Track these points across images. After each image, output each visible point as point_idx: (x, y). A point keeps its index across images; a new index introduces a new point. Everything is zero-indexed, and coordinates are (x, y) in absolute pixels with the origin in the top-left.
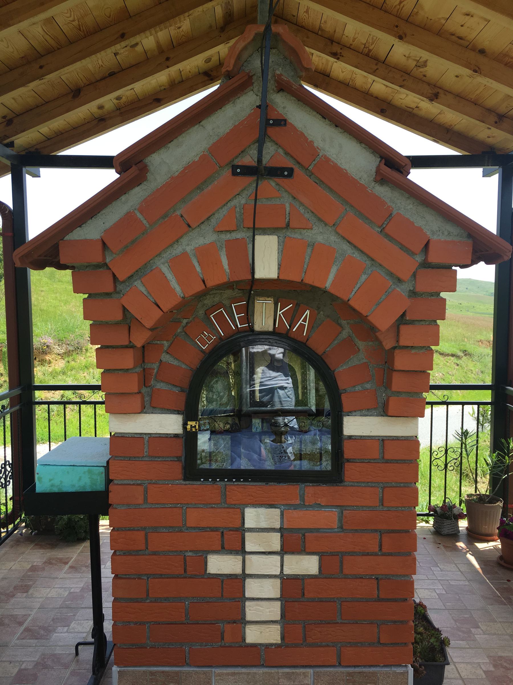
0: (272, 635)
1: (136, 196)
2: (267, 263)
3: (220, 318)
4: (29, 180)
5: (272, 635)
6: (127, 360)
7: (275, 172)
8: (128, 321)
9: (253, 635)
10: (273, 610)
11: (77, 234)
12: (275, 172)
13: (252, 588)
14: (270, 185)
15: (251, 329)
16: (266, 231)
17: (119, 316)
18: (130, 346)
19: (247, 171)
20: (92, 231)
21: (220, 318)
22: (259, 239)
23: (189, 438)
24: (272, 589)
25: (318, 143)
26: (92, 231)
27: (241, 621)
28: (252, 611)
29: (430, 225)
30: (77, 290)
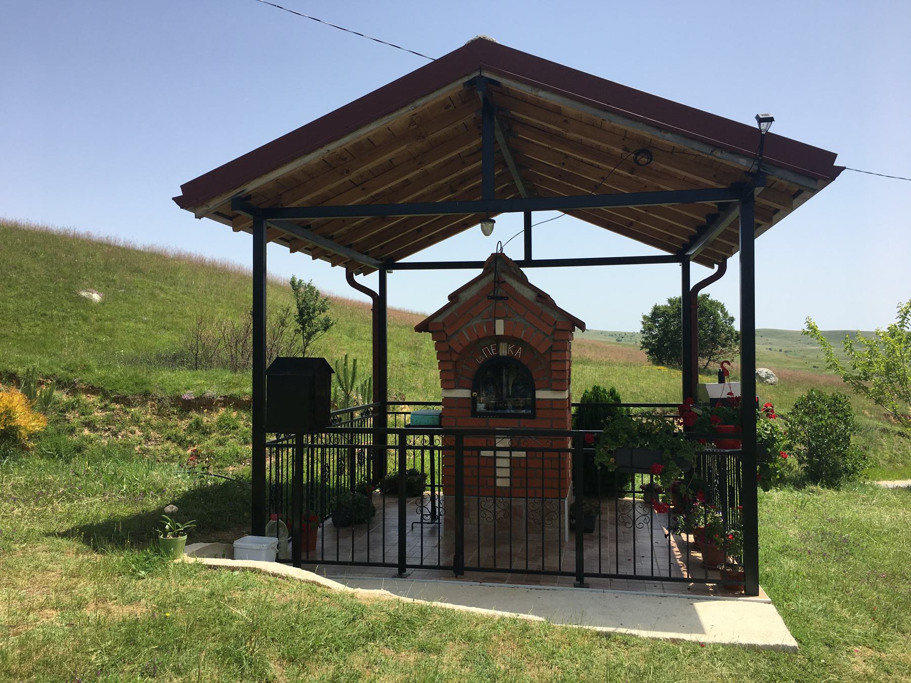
0: (506, 483)
1: (455, 307)
2: (500, 328)
3: (486, 351)
4: (388, 275)
5: (506, 483)
6: (450, 366)
7: (502, 298)
8: (451, 350)
9: (499, 483)
10: (507, 473)
11: (435, 320)
12: (502, 298)
13: (499, 463)
14: (500, 303)
15: (498, 355)
16: (499, 318)
17: (448, 348)
18: (451, 360)
19: (492, 298)
20: (439, 320)
21: (486, 351)
22: (497, 321)
23: (474, 401)
24: (506, 463)
25: (516, 288)
26: (439, 320)
27: (495, 477)
28: (499, 473)
29: (555, 316)
30: (670, 301)
